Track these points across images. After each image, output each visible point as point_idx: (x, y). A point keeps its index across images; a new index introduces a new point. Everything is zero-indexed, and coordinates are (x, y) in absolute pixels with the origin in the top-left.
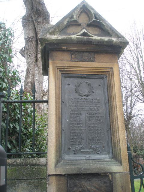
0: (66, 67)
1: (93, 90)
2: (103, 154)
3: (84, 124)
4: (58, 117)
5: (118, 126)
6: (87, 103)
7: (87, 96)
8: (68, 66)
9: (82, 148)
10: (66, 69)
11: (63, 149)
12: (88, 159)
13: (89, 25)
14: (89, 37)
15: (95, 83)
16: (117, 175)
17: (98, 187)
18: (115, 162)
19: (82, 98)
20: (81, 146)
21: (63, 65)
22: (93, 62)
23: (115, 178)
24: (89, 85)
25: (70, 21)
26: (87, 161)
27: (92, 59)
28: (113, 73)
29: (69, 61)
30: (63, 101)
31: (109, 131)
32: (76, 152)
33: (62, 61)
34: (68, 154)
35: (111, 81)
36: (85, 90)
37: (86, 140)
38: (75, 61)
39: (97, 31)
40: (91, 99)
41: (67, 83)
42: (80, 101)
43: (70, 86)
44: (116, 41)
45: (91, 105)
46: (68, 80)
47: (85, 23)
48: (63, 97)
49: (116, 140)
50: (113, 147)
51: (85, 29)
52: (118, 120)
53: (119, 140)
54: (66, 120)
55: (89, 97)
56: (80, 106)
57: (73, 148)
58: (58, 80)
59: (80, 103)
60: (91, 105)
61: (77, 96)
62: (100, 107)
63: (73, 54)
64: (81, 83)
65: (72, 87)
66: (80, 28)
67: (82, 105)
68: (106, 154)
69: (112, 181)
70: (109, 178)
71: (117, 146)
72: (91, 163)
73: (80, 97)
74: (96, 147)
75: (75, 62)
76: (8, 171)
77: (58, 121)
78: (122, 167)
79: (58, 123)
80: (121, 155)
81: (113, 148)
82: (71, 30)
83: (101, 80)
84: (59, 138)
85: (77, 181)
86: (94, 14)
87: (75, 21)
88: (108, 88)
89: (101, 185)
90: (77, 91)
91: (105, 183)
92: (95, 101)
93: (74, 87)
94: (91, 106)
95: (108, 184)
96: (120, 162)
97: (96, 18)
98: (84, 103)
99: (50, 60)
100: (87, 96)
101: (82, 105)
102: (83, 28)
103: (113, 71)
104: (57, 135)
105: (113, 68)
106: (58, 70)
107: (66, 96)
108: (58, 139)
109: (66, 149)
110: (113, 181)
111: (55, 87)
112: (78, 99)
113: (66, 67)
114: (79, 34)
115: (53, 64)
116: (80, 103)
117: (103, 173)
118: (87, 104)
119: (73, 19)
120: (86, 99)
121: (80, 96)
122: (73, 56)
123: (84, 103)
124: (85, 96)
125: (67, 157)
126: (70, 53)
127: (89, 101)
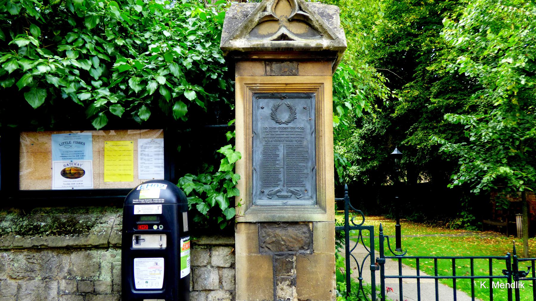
0: (258, 85)
1: (295, 114)
2: (304, 199)
3: (282, 161)
4: (248, 152)
5: (325, 165)
6: (286, 133)
7: (287, 123)
8: (260, 84)
9: (279, 191)
10: (258, 88)
11: (254, 193)
12: (285, 204)
13: (292, 20)
14: (289, 42)
15: (299, 104)
16: (319, 224)
17: (295, 237)
18: (319, 210)
19: (281, 126)
20: (277, 189)
21: (254, 82)
22: (296, 75)
23: (316, 228)
24: (290, 107)
25: (262, 17)
26: (283, 208)
27: (294, 71)
28: (324, 91)
29: (262, 76)
30: (255, 131)
31: (314, 170)
32: (270, 196)
33: (252, 76)
34: (260, 199)
35: (320, 102)
36: (285, 116)
37: (284, 181)
38: (271, 75)
39: (300, 28)
40: (292, 128)
41: (261, 106)
42: (277, 130)
43: (264, 110)
44: (328, 47)
45: (292, 136)
46: (263, 102)
47: (285, 16)
48: (254, 125)
49: (321, 182)
50: (317, 190)
51: (286, 27)
52: (326, 156)
53: (325, 182)
54: (258, 156)
55: (290, 125)
56: (277, 138)
57: (267, 191)
58: (248, 104)
59: (277, 133)
60: (292, 136)
61: (274, 124)
62: (303, 138)
63: (268, 64)
64: (279, 106)
65: (267, 111)
66: (275, 26)
67: (280, 136)
68: (308, 199)
69: (312, 231)
70: (309, 228)
71: (322, 190)
72: (310, 210)
73: (278, 126)
74: (296, 190)
75: (270, 77)
76: (425, 275)
77: (248, 158)
78: (326, 215)
79: (248, 161)
80: (325, 201)
81: (317, 192)
82: (265, 29)
83: (308, 101)
84: (249, 178)
85: (270, 230)
86: (298, 3)
87: (271, 16)
88: (316, 112)
89: (299, 235)
90: (273, 117)
91: (304, 233)
92: (297, 130)
93: (270, 112)
94: (291, 137)
95: (308, 235)
96: (324, 209)
97: (300, 9)
98: (282, 133)
99: (236, 75)
100: (287, 123)
101: (280, 136)
102: (282, 26)
103: (324, 88)
104: (246, 175)
105: (323, 83)
106: (248, 89)
107: (259, 125)
108: (248, 180)
109: (258, 193)
110: (314, 232)
111: (244, 112)
112: (275, 128)
113: (258, 85)
114: (275, 37)
115: (241, 80)
116: (277, 133)
117: (301, 222)
118: (286, 135)
119: (266, 13)
120: (285, 128)
121: (277, 124)
122: (268, 68)
123: (282, 133)
124: (284, 123)
125: (259, 202)
126: (263, 63)
127: (289, 130)
